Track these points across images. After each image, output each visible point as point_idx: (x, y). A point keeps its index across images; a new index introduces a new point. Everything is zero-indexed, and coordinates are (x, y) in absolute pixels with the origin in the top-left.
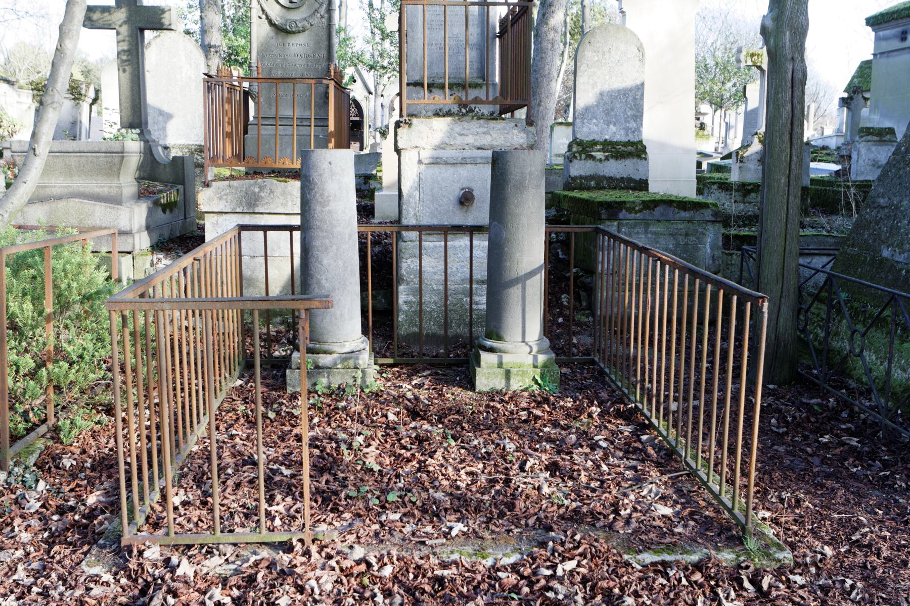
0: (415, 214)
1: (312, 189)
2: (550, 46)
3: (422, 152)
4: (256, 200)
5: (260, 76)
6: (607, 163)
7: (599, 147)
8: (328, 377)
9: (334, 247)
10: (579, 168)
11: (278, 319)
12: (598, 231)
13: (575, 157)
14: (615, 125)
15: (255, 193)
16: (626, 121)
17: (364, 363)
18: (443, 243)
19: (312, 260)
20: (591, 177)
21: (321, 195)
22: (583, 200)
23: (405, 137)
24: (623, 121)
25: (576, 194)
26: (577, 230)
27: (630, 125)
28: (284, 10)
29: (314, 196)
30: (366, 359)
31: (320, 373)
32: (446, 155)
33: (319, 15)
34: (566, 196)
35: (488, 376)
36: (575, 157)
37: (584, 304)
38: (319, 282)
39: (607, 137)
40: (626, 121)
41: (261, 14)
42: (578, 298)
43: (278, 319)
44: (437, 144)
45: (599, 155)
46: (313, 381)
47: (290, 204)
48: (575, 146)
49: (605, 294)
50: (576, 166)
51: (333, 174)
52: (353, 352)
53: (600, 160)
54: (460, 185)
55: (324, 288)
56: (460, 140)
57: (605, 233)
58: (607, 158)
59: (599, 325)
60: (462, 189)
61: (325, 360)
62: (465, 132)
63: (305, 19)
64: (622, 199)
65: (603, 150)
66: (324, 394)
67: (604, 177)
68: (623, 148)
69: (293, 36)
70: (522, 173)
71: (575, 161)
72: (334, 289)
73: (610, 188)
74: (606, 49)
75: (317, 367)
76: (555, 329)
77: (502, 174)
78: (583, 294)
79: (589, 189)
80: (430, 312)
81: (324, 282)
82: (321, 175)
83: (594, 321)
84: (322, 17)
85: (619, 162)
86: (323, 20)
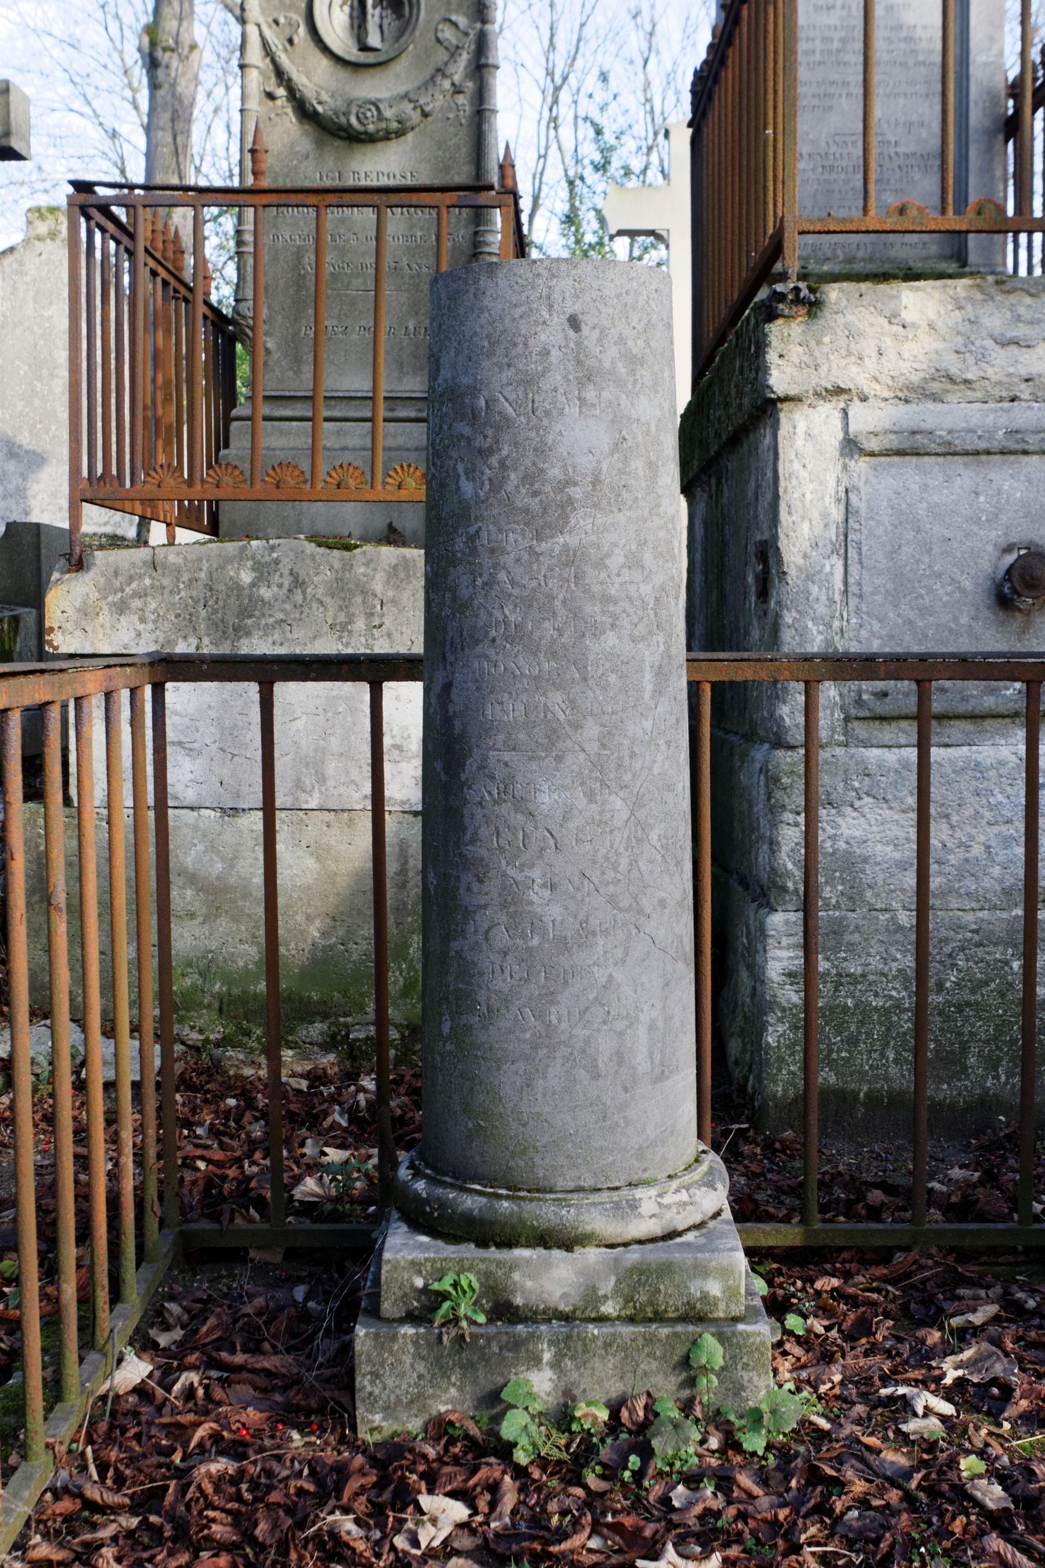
1: (485, 453)
3: (856, 410)
4: (244, 613)
5: (266, 183)
8: (556, 1365)
9: (592, 730)
11: (317, 1030)
15: (238, 587)
17: (731, 1293)
18: (912, 754)
19: (483, 791)
21: (528, 479)
23: (796, 352)
28: (343, 74)
29: (496, 485)
30: (728, 1274)
31: (516, 1344)
32: (948, 422)
33: (447, 84)
38: (512, 900)
41: (272, 86)
43: (317, 1030)
44: (916, 378)
46: (486, 1381)
47: (360, 624)
51: (588, 375)
52: (671, 1235)
54: (996, 535)
55: (536, 925)
56: (1000, 364)
60: (1008, 549)
61: (549, 1278)
62: (1020, 331)
63: (406, 96)
66: (543, 1462)
69: (369, 149)
72: (586, 933)
75: (503, 1310)
80: (886, 1012)
81: (537, 896)
82: (528, 382)
84: (457, 90)
86: (461, 99)
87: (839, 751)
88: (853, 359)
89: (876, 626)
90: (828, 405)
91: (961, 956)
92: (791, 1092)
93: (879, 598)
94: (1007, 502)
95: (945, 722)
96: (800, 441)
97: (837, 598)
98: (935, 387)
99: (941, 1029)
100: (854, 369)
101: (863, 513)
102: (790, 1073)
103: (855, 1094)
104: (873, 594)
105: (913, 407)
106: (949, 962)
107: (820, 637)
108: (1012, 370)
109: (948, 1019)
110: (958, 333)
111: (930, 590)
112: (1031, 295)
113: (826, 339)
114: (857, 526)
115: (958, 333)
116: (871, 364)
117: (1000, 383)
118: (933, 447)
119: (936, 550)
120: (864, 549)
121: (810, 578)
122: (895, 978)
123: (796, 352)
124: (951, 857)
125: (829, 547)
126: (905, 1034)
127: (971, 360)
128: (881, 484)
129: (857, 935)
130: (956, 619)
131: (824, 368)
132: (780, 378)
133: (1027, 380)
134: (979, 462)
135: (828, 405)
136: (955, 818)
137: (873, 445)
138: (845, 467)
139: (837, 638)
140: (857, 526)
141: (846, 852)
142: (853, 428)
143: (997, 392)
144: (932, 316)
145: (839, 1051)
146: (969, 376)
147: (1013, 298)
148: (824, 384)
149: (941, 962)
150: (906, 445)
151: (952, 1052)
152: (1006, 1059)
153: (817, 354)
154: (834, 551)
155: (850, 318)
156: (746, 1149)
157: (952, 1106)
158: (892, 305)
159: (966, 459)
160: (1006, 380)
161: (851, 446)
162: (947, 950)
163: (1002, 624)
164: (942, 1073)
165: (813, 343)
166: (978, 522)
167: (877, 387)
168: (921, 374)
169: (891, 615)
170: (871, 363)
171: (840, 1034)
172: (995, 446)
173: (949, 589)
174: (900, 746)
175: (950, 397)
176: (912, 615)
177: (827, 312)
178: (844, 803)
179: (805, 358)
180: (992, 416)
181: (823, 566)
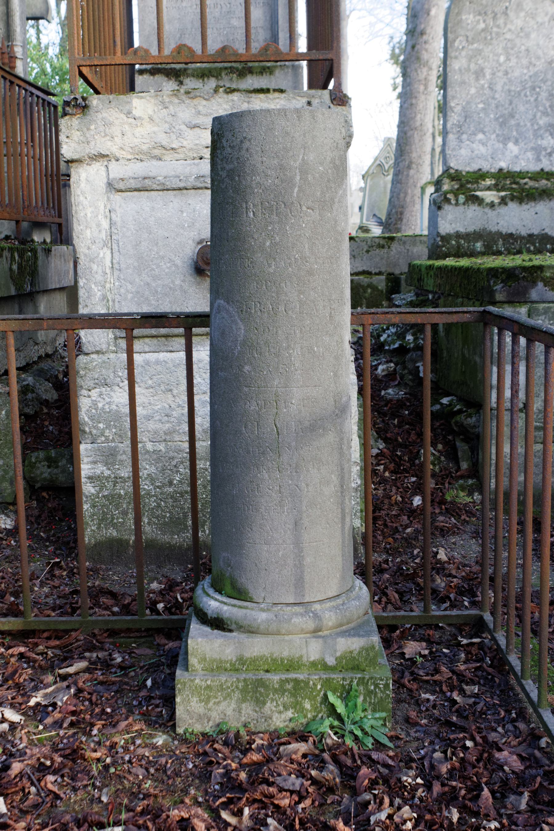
0: (104, 297)
2: (422, 88)
6: (503, 210)
7: (489, 182)
10: (458, 220)
12: (486, 319)
13: (448, 201)
14: (516, 142)
16: (537, 135)
20: (477, 236)
22: (460, 269)
23: (76, 135)
24: (530, 135)
25: (450, 262)
26: (436, 319)
27: (544, 143)
34: (430, 267)
35: (206, 695)
36: (448, 201)
37: (464, 465)
39: (503, 165)
40: (537, 135)
42: (452, 454)
45: (490, 196)
48: (446, 181)
49: (507, 449)
50: (450, 217)
53: (492, 205)
57: (505, 323)
58: (503, 201)
59: (495, 508)
64: (536, 263)
65: (496, 187)
67: (499, 234)
68: (531, 183)
70: (282, 167)
71: (446, 207)
73: (509, 253)
74: (499, 9)
76: (389, 556)
77: (231, 174)
78: (462, 447)
79: (472, 254)
83: (482, 502)
85: (525, 207)
87: (112, 356)
88: (108, 138)
89: (129, 287)
90: (98, 164)
91: (182, 466)
92: (93, 541)
93: (130, 271)
94: (199, 216)
95: (169, 339)
96: (83, 185)
97: (108, 271)
98: (157, 152)
99: (173, 506)
100: (109, 143)
101: (119, 224)
102: (92, 530)
103: (127, 542)
104: (127, 269)
105: (145, 163)
106: (175, 469)
107: (99, 293)
108: (197, 142)
109: (176, 500)
110: (166, 122)
111: (158, 266)
112: (206, 99)
113: (92, 127)
114: (116, 231)
115: (166, 122)
116: (118, 140)
117: (191, 149)
118: (155, 187)
119: (160, 244)
120: (121, 244)
121: (92, 260)
122: (146, 479)
123: (76, 135)
124: (174, 413)
125: (102, 243)
126: (153, 509)
127: (174, 137)
128: (129, 207)
129: (124, 456)
130: (173, 282)
131: (93, 143)
132: (68, 150)
133: (346, 121)
134: (182, 194)
135: (98, 164)
136: (175, 392)
137: (121, 186)
138: (108, 199)
139: (108, 293)
140: (116, 231)
141: (116, 411)
142: (111, 176)
143: (191, 154)
144: (150, 112)
145: (118, 518)
146: (174, 146)
147: (196, 101)
148: (93, 152)
149: (170, 470)
150: (139, 186)
151: (179, 518)
152: (209, 521)
153: (88, 135)
154: (105, 245)
155: (105, 115)
156: (57, 572)
157: (180, 547)
158: (127, 107)
159: (175, 192)
160: (195, 147)
161: (112, 187)
162: (174, 463)
163: (199, 284)
164: (174, 530)
165: (85, 129)
166: (183, 227)
167: (124, 153)
168: (147, 146)
169: (137, 280)
170: (118, 140)
171: (118, 509)
172: (189, 185)
173: (169, 265)
174: (146, 352)
175: (165, 157)
176: (149, 280)
177: (91, 112)
178: (114, 384)
179: (81, 138)
180: (189, 168)
181: (99, 254)
